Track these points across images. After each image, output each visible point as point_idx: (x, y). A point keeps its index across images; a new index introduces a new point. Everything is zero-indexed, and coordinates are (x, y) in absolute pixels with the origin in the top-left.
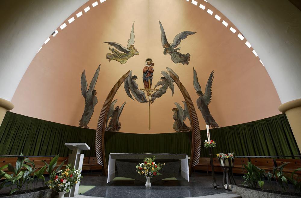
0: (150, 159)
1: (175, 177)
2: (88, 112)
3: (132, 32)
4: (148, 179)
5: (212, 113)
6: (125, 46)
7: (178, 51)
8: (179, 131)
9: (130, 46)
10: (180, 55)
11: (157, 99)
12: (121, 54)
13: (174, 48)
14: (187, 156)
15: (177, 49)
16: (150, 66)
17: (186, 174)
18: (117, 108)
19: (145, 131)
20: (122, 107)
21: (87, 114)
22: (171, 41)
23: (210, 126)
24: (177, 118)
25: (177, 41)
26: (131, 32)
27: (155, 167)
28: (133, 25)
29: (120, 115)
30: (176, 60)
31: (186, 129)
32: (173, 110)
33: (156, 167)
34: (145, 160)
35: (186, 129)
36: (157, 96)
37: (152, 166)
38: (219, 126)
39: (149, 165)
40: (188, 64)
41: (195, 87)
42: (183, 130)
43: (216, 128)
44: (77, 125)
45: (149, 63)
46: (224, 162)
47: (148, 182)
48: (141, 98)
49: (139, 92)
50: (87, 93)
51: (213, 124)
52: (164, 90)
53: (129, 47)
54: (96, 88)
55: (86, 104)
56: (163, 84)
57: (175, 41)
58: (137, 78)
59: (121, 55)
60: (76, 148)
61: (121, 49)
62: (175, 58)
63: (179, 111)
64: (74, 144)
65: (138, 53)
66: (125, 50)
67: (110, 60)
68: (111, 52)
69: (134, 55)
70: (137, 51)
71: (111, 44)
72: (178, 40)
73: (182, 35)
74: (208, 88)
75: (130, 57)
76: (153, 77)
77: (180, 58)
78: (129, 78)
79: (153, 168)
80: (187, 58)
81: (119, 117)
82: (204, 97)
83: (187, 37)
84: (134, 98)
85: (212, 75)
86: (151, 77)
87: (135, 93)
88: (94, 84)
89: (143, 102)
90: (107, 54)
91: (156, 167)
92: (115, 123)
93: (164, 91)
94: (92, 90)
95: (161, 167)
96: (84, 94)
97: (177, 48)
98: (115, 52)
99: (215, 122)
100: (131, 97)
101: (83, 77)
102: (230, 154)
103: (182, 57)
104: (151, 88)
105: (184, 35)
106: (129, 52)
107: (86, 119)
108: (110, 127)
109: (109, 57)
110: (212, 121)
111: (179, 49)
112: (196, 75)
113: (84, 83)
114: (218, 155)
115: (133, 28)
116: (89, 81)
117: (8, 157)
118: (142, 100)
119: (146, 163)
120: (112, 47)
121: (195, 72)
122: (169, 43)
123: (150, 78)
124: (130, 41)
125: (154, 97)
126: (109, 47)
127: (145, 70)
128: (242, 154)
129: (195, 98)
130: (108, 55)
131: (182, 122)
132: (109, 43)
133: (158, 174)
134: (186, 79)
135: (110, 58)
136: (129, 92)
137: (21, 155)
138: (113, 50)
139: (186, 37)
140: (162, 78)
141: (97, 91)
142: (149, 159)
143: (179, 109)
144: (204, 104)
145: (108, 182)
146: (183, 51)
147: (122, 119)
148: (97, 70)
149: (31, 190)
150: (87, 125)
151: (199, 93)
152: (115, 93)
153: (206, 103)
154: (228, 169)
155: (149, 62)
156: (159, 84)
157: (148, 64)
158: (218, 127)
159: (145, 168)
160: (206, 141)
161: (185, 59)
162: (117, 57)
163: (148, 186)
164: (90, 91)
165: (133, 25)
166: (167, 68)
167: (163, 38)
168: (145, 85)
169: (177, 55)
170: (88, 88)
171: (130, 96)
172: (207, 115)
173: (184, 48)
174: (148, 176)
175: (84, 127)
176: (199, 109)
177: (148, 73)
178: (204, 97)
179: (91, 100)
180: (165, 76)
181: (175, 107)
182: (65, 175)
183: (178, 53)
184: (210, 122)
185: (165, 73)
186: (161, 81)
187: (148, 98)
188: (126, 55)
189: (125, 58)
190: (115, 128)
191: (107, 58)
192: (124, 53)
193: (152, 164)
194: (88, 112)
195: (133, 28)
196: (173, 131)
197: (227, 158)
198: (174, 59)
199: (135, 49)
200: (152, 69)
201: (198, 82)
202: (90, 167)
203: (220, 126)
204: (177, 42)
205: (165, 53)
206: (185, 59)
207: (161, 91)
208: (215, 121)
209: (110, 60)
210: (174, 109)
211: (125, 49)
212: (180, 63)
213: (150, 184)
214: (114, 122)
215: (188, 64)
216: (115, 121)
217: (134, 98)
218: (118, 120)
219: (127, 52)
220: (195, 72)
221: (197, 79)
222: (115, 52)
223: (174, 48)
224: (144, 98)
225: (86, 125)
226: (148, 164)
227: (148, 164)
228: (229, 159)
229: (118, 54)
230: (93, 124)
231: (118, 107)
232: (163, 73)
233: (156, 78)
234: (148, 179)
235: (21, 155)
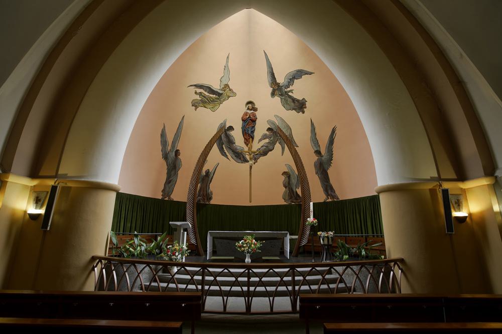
0: (250, 237)
1: (279, 257)
2: (171, 179)
3: (226, 67)
4: (248, 255)
5: (333, 181)
6: (216, 87)
7: (290, 94)
8: (289, 202)
9: (223, 86)
10: (294, 100)
11: (262, 159)
12: (211, 97)
13: (286, 90)
14: (288, 234)
15: (289, 91)
16: (252, 111)
17: (287, 251)
18: (208, 172)
19: (247, 203)
20: (214, 170)
21: (170, 182)
22: (281, 80)
23: (329, 197)
24: (288, 185)
25: (289, 80)
26: (225, 67)
27: (255, 244)
28: (228, 57)
29: (211, 181)
30: (288, 107)
31: (299, 201)
32: (282, 174)
33: (255, 244)
34: (245, 238)
35: (299, 201)
36: (261, 155)
37: (252, 244)
38: (339, 198)
39: (248, 242)
40: (303, 112)
41: (313, 145)
42: (295, 201)
43: (335, 200)
44: (160, 197)
45: (250, 108)
46: (323, 240)
47: (248, 258)
48: (239, 156)
49: (236, 149)
50: (169, 155)
51: (332, 196)
52: (271, 146)
53: (221, 87)
55: (168, 168)
56: (270, 138)
57: (286, 80)
58: (233, 129)
59: (212, 99)
60: (181, 226)
61: (212, 91)
62: (287, 104)
63: (291, 176)
64: (179, 223)
65: (235, 94)
66: (217, 92)
67: (196, 107)
68: (198, 97)
69: (229, 97)
70: (233, 92)
71: (197, 86)
72: (290, 79)
73: (296, 74)
74: (329, 147)
75: (224, 100)
76: (256, 127)
77: (293, 104)
78: (223, 130)
79: (253, 245)
80: (303, 105)
81: (210, 183)
82: (323, 158)
83: (303, 77)
84: (229, 157)
85: (333, 131)
86: (254, 127)
87: (231, 149)
88: (177, 142)
89: (242, 163)
90: (193, 100)
91: (255, 244)
92: (205, 193)
93: (271, 147)
94: (175, 150)
95: (261, 244)
96: (165, 156)
97: (288, 89)
98: (203, 96)
99: (335, 193)
100: (226, 156)
101: (163, 135)
102: (331, 233)
103: (296, 102)
104: (252, 150)
105: (299, 74)
106: (222, 94)
107: (169, 188)
108: (199, 198)
109: (195, 105)
110: (332, 192)
111: (291, 91)
112: (314, 129)
113: (164, 142)
114: (318, 233)
115: (227, 62)
116: (170, 138)
117: (130, 234)
118: (240, 159)
119: (246, 241)
120: (199, 90)
121: (312, 124)
122: (278, 81)
123: (252, 129)
124: (223, 79)
125: (257, 156)
126: (196, 91)
127: (245, 117)
128: (347, 233)
129: (309, 161)
130: (193, 102)
131: (295, 191)
132: (195, 85)
133: (257, 250)
134: (301, 136)
135: (197, 105)
136: (223, 148)
137: (136, 233)
138: (200, 94)
139: (301, 77)
140: (269, 129)
141: (180, 151)
142: (248, 237)
143: (291, 174)
144: (323, 169)
146: (297, 95)
147: (213, 187)
148: (179, 125)
150: (171, 196)
151: (318, 153)
152: (206, 157)
153: (326, 166)
154: (326, 247)
155: (250, 105)
157: (248, 109)
158: (338, 199)
159: (245, 245)
160: (308, 219)
161: (300, 106)
162: (206, 102)
163: (248, 262)
164: (172, 152)
165: (228, 57)
167: (270, 75)
168: (245, 138)
169: (289, 100)
170: (169, 148)
171: (224, 154)
172: (326, 183)
173: (298, 90)
174: (248, 252)
175: (167, 199)
176: (316, 174)
177: (249, 122)
178: (323, 158)
179: (174, 164)
180: (273, 127)
181: (287, 170)
182: (175, 250)
183: (290, 97)
184: (329, 192)
185: (273, 123)
186: (267, 133)
188: (218, 99)
189: (216, 103)
190: (206, 198)
191: (193, 106)
192: (215, 96)
193: (252, 241)
194: (171, 179)
195: (227, 62)
196: (283, 202)
197: (325, 237)
198: (285, 104)
199: (230, 90)
200: (254, 115)
201: (316, 139)
203: (341, 198)
204: (289, 82)
205: (273, 94)
206: (300, 106)
207: (267, 147)
208: (335, 191)
209: (196, 107)
210: (284, 173)
211: (216, 90)
212: (294, 111)
213: (250, 260)
214: (204, 191)
215: (303, 112)
216: (205, 190)
217: (229, 157)
218: (209, 187)
219: (219, 95)
220: (312, 124)
221: (316, 134)
222: (203, 96)
223: (286, 90)
224: (243, 157)
225: (169, 196)
226: (247, 241)
227: (247, 241)
228: (328, 237)
229: (207, 99)
230: (181, 193)
231: (208, 170)
232: (269, 122)
233: (261, 129)
234: (248, 255)
235: (136, 233)
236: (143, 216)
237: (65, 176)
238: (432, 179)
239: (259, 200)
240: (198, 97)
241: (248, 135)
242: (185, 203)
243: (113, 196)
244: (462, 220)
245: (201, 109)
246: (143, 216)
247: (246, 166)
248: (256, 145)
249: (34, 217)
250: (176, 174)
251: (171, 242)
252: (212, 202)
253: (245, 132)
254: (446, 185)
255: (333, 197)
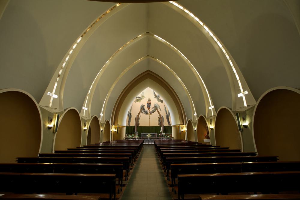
10: (160, 100)
11: (152, 113)
33: (150, 136)
48: (146, 113)
54: (131, 112)
61: (139, 98)
65: (145, 97)
68: (136, 100)
76: (151, 105)
91: (150, 136)
93: (155, 111)
125: (151, 113)
140: (154, 106)
145: (154, 35)
149: (217, 147)
151: (166, 113)
156: (153, 108)
166: (156, 103)
177: (149, 104)
185: (155, 105)
187: (149, 113)
202: (172, 183)
205: (155, 97)
219: (141, 98)
232: (154, 104)
233: (152, 106)
236: (184, 146)
237: (119, 125)
238: (179, 125)
239: (152, 125)
240: (136, 100)
241: (149, 108)
242: (134, 127)
243: (125, 127)
244: (182, 131)
245: (136, 102)
246: (184, 146)
247: (148, 116)
248: (151, 110)
249: (115, 132)
250: (131, 119)
251: (135, 135)
252: (140, 126)
253: (148, 107)
254: (181, 126)
255: (170, 124)
